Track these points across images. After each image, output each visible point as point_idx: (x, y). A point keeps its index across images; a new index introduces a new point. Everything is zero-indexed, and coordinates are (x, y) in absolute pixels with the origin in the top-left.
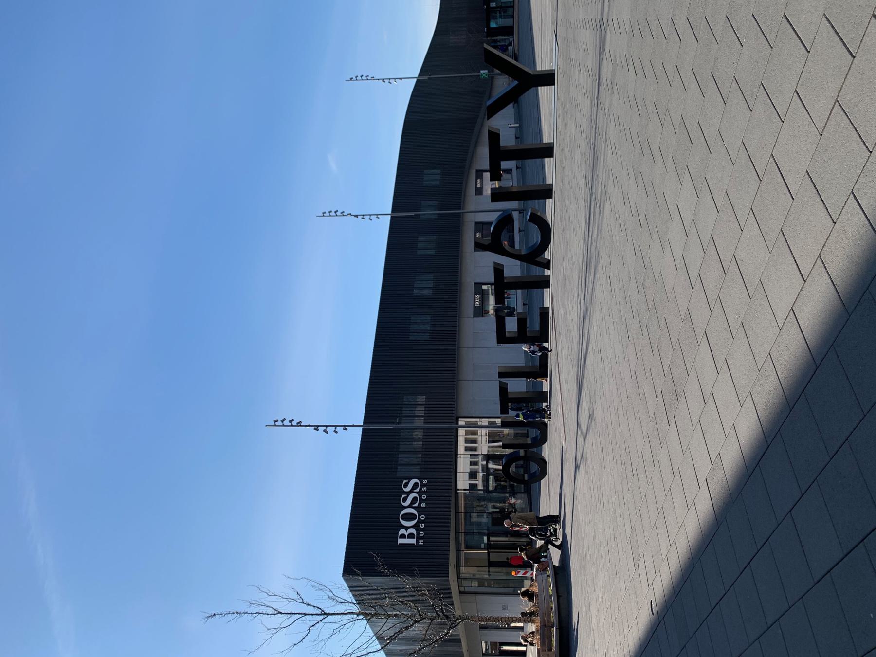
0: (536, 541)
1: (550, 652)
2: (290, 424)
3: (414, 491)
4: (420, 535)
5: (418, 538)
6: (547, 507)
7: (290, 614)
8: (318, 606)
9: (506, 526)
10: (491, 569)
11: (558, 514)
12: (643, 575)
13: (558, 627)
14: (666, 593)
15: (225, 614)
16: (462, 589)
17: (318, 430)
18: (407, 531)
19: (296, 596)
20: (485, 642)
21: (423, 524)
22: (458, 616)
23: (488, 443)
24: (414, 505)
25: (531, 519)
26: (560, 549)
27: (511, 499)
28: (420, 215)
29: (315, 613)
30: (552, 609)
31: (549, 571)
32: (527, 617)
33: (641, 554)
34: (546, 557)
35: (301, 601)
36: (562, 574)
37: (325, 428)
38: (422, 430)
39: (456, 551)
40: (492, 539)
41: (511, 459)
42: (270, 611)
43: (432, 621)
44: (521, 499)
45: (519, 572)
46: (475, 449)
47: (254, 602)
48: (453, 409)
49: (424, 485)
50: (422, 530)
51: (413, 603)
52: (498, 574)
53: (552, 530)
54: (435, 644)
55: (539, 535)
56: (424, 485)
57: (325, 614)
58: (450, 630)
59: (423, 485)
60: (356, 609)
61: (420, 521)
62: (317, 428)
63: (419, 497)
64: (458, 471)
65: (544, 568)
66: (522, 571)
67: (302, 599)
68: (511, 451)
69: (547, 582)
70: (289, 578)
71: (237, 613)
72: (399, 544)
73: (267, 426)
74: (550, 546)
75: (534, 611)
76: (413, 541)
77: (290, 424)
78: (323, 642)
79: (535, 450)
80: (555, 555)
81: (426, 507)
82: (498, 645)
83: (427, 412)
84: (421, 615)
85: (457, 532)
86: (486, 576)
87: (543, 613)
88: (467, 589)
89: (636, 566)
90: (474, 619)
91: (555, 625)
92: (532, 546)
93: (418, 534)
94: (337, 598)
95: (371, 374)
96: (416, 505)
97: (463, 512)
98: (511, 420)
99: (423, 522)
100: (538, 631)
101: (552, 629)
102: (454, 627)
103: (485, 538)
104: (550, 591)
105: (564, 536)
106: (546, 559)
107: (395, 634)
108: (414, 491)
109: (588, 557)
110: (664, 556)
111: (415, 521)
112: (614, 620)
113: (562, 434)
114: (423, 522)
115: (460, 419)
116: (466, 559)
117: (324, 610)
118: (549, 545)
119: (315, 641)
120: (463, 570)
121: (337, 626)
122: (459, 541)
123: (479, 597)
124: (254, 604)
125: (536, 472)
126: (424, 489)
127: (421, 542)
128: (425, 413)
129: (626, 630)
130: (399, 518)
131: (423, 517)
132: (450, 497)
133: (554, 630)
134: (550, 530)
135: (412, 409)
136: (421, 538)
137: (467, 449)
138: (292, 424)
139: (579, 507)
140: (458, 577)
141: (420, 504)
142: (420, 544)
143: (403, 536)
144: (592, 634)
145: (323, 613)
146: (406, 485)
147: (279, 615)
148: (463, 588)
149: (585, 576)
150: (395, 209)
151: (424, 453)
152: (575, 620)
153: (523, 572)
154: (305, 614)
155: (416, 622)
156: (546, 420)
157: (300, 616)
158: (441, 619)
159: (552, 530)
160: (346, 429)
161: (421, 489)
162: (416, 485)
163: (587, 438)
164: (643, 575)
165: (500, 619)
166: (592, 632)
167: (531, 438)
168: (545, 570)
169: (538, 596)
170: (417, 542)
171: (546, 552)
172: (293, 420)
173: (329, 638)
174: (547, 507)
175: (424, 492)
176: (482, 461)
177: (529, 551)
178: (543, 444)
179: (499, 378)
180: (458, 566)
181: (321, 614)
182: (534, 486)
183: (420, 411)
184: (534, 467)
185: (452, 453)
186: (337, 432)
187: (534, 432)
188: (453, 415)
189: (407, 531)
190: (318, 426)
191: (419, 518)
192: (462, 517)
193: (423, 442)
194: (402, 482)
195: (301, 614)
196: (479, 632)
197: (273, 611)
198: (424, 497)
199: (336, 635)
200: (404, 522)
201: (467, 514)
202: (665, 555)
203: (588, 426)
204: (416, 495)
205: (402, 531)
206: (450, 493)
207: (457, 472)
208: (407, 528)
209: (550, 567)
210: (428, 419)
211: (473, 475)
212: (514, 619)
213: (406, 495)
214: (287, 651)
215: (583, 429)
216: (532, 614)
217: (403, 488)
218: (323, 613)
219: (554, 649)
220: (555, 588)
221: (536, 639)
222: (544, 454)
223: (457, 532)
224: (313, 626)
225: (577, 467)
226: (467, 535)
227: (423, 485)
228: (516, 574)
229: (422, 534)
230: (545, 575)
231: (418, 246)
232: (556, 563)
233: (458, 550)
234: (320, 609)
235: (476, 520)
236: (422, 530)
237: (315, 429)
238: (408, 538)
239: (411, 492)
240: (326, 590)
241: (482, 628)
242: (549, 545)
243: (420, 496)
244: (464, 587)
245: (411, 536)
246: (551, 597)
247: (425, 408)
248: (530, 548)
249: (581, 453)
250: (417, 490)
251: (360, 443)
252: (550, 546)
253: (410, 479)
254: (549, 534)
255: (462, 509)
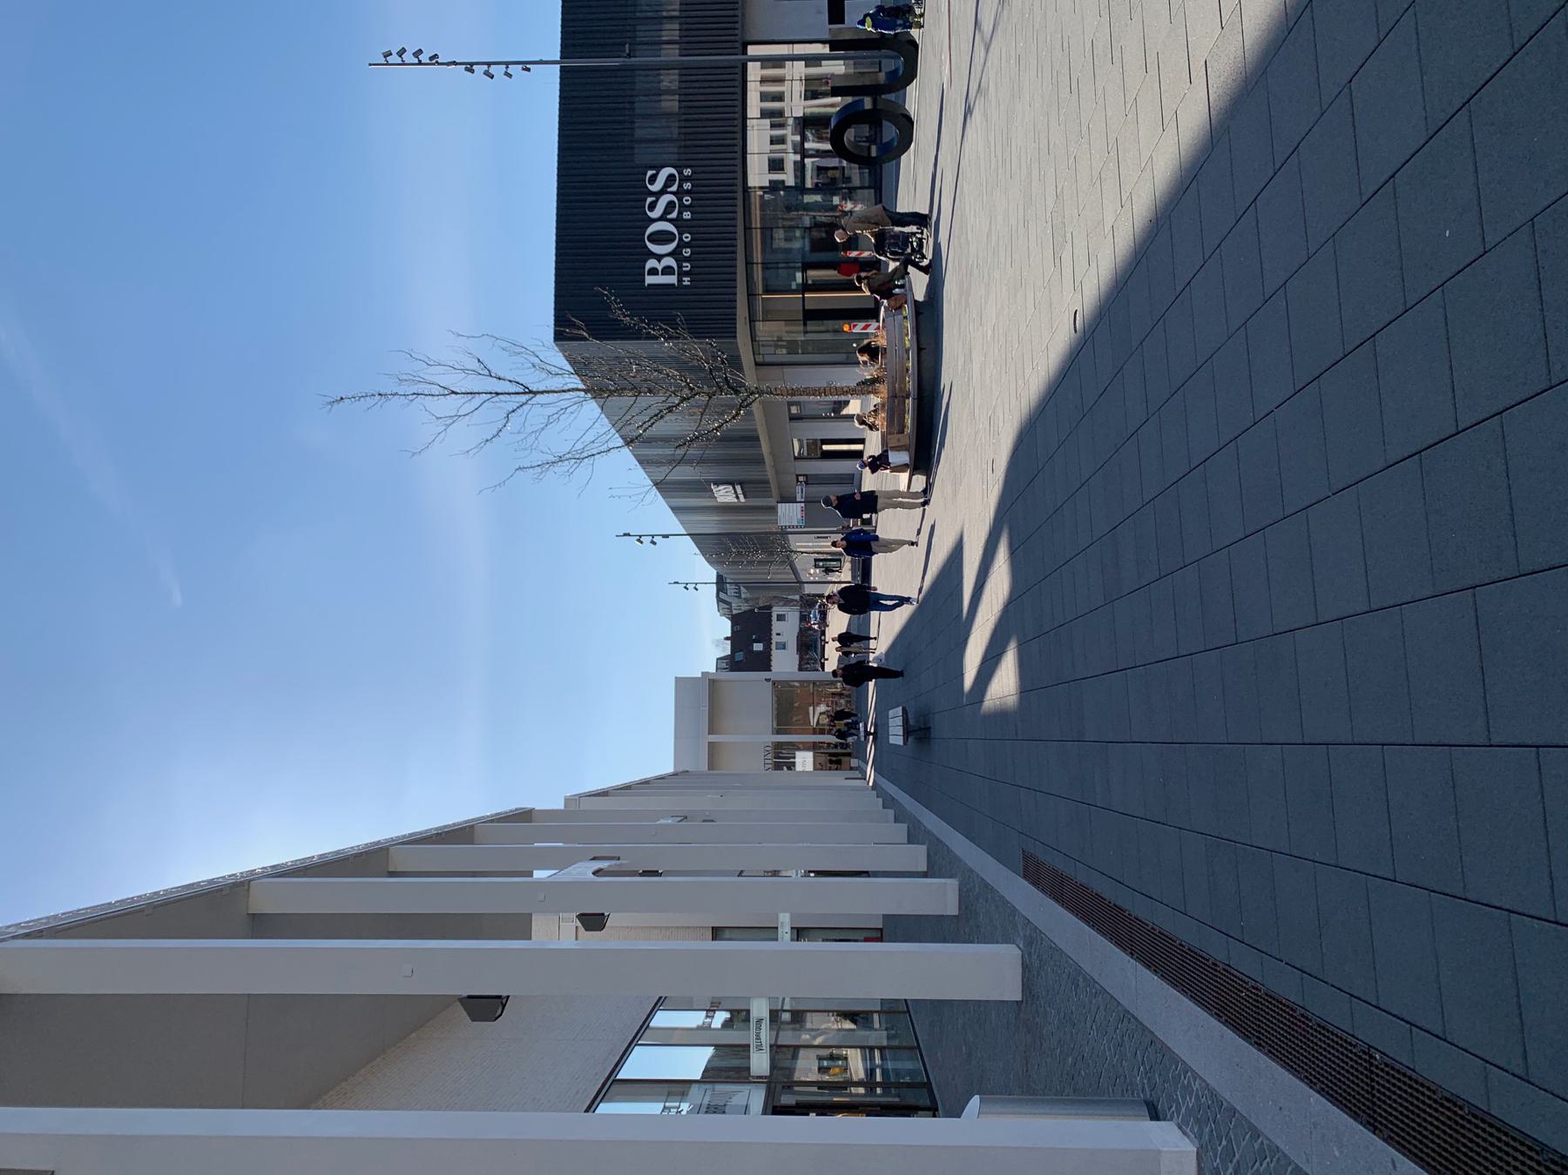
0: (887, 265)
1: (900, 435)
2: (416, 61)
3: (669, 190)
4: (684, 269)
5: (681, 274)
6: (909, 199)
7: (471, 393)
8: (517, 380)
9: (838, 241)
10: (812, 326)
11: (927, 212)
12: (1067, 271)
13: (916, 397)
14: (1103, 288)
15: (360, 397)
16: (760, 359)
17: (472, 71)
18: (659, 261)
19: (475, 365)
20: (799, 440)
21: (689, 250)
22: (753, 389)
23: (805, 100)
24: (669, 217)
25: (877, 216)
26: (926, 273)
27: (846, 203)
28: (632, 69)
29: (513, 391)
30: (907, 370)
31: (907, 310)
32: (867, 387)
33: (1069, 235)
34: (902, 286)
35: (487, 373)
36: (929, 315)
37: (486, 67)
38: (677, 71)
39: (748, 295)
40: (811, 273)
41: (849, 117)
42: (435, 390)
43: (710, 398)
44: (863, 201)
45: (855, 326)
46: (780, 113)
47: (405, 377)
48: (737, 26)
49: (687, 179)
50: (687, 259)
51: (676, 370)
52: (820, 332)
53: (915, 244)
54: (717, 431)
55: (893, 253)
56: (687, 179)
57: (531, 392)
58: (740, 410)
59: (684, 179)
60: (576, 382)
61: (681, 245)
62: (470, 67)
63: (678, 200)
64: (749, 151)
65: (898, 305)
66: (860, 324)
67: (489, 370)
68: (849, 99)
69: (902, 327)
70: (459, 335)
71: (380, 394)
72: (649, 285)
73: (370, 65)
74: (910, 269)
75: (878, 377)
76: (672, 279)
77: (416, 61)
78: (534, 435)
79: (891, 97)
80: (919, 283)
81: (692, 219)
82: (819, 443)
83: (684, 33)
84: (692, 389)
85: (749, 263)
86: (801, 338)
87: (893, 377)
88: (768, 359)
89: (1057, 259)
90: (778, 392)
91: (912, 394)
92: (879, 269)
93: (680, 267)
94: (548, 367)
95: (560, 129)
96: (674, 215)
97: (759, 226)
98: (847, 37)
99: (687, 245)
100: (883, 405)
101: (907, 401)
102: (747, 406)
103: (799, 275)
104: (907, 342)
105: (937, 248)
106: (903, 290)
107: (651, 418)
108: (669, 190)
109: (976, 271)
110: (1108, 228)
111: (673, 245)
112: (1009, 360)
113: (945, 57)
114: (687, 245)
115: (749, 47)
116: (766, 312)
117: (528, 386)
118: (909, 266)
119: (519, 432)
120: (760, 326)
121: (551, 410)
122: (753, 279)
123: (787, 370)
124: (406, 380)
125: (892, 140)
126: (688, 186)
127: (686, 281)
128: (680, 37)
129: (1028, 371)
130: (644, 241)
131: (687, 237)
132: (736, 172)
133: (910, 402)
134: (912, 243)
135: (655, 27)
136: (687, 274)
137: (765, 114)
138: (420, 61)
139: (966, 188)
140: (753, 339)
141: (680, 213)
142: (684, 283)
143: (653, 272)
144: (971, 396)
145: (527, 390)
146: (653, 179)
147: (453, 395)
148: (761, 356)
149: (967, 305)
150: (570, 44)
151: (683, 143)
152: (942, 387)
153: (861, 325)
154: (497, 394)
155: (683, 400)
156: (914, 32)
157: (489, 396)
158: (726, 394)
159: (915, 244)
160: (529, 70)
161: (680, 186)
162: (671, 178)
163: (992, 46)
164: (1067, 271)
165: (822, 390)
166: (972, 392)
167: (886, 73)
168: (900, 307)
169: (886, 353)
170: (680, 281)
171: (903, 278)
172: (420, 51)
173: (543, 429)
174: (909, 199)
175: (688, 192)
176: (792, 134)
177: (873, 279)
178: (908, 85)
179: (830, 23)
180: (752, 320)
181: (525, 393)
182: (887, 167)
183: (671, 31)
184: (890, 132)
185: (736, 89)
186: (510, 76)
187: (892, 63)
188: (737, 38)
189: (659, 261)
190: (472, 64)
191: (681, 239)
192: (757, 236)
193: (680, 95)
194: (646, 174)
195: (491, 393)
196: (788, 425)
197: (442, 391)
198: (687, 200)
199: (553, 424)
200: (656, 246)
201: (767, 231)
202: (1110, 226)
203: (995, 19)
204: (673, 198)
205: (651, 263)
206: (734, 179)
207: (747, 81)
208: (659, 258)
209: (909, 301)
210: (687, 44)
211: (776, 165)
212: (845, 389)
213: (654, 172)
214: (475, 450)
215: (985, 29)
216: (874, 381)
217: (648, 212)
218: (527, 390)
219: (908, 430)
220: (915, 337)
221: (881, 421)
222: (910, 107)
223: (749, 263)
224: (513, 411)
225: (968, 112)
226: (767, 268)
227: (684, 179)
228: (850, 329)
229: (687, 266)
230: (901, 317)
231: (636, 136)
232: (920, 295)
233: (751, 295)
234: (522, 385)
235: (784, 245)
236: (687, 259)
237: (467, 69)
238: (662, 274)
239: (663, 192)
240: (527, 354)
241: (793, 418)
242: (909, 266)
243: (680, 200)
244: (763, 355)
245: (668, 271)
246: (907, 351)
247: (680, 24)
248: (875, 274)
249: (978, 81)
250: (674, 188)
251: (554, 258)
252: (910, 269)
253: (659, 168)
254: (909, 250)
255: (756, 222)
